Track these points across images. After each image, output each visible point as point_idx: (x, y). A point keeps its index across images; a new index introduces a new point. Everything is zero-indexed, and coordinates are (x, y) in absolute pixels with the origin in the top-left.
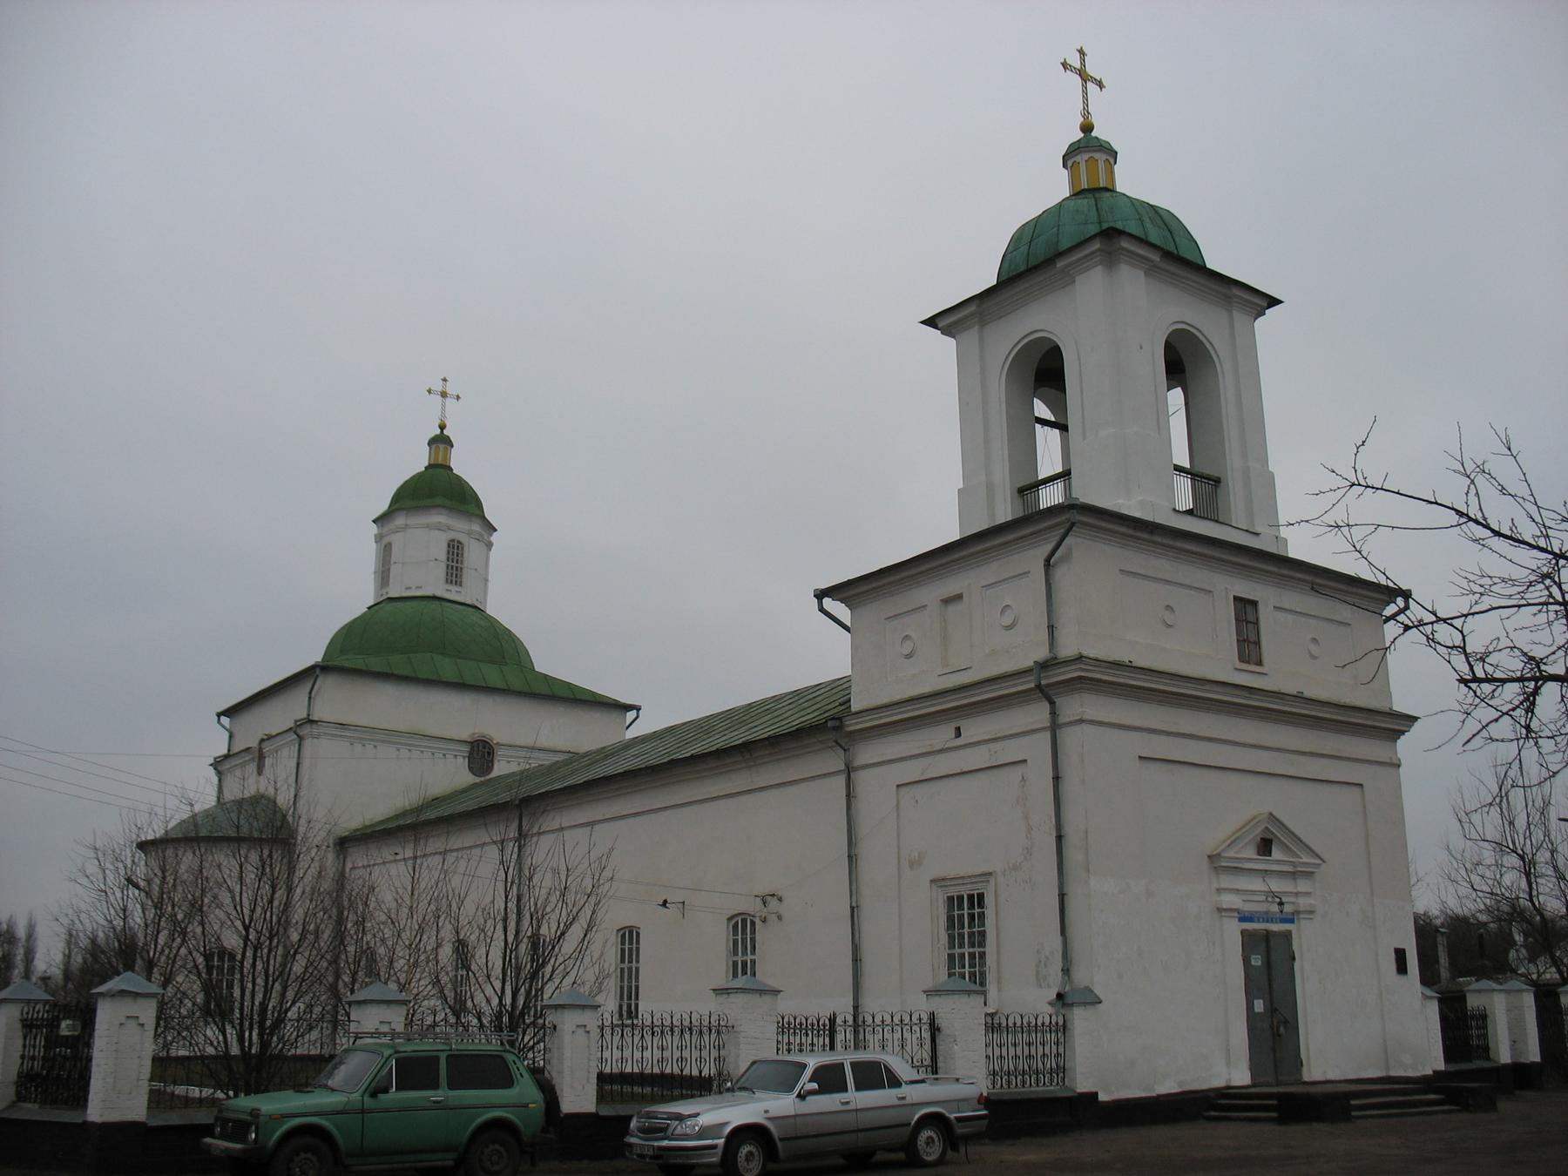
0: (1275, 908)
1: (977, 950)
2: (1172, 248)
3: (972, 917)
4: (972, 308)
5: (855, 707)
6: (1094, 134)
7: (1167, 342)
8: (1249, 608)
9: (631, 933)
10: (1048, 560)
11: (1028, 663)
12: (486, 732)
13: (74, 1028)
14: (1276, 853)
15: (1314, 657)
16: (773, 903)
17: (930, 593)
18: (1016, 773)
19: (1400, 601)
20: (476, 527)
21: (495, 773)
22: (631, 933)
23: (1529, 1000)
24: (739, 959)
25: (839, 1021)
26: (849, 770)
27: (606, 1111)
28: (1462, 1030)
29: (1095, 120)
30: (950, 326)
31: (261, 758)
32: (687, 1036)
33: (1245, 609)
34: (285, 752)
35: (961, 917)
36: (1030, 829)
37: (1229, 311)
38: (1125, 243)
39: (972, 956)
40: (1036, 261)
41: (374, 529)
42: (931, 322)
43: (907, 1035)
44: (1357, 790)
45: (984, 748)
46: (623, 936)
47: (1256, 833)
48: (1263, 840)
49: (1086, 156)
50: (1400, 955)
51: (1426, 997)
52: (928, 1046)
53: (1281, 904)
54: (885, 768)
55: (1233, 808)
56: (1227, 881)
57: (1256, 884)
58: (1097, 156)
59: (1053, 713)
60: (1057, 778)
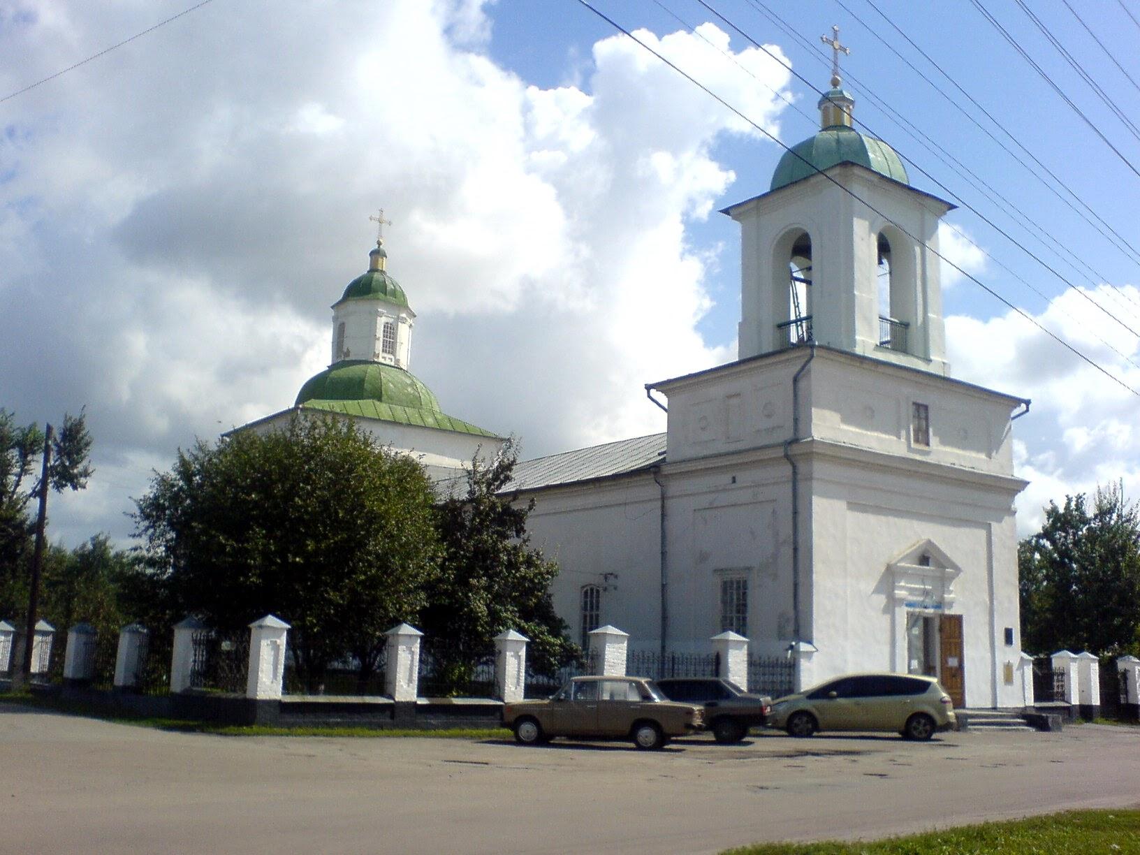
4: (752, 205)
10: (795, 380)
11: (781, 440)
19: (1023, 406)
23: (1095, 667)
28: (1046, 683)
30: (740, 214)
42: (726, 211)
50: (1008, 635)
59: (795, 473)
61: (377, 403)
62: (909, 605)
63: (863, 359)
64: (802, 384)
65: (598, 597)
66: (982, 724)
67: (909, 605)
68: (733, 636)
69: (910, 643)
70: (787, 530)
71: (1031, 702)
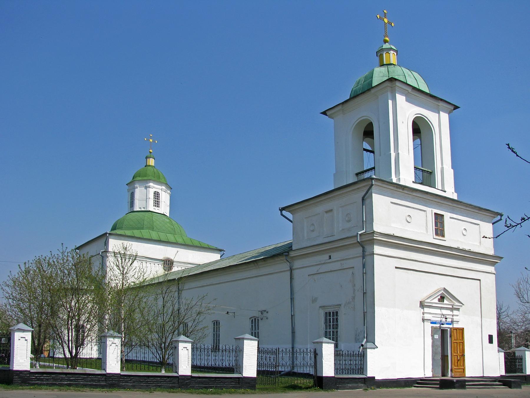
0: (444, 320)
1: (335, 330)
2: (416, 86)
3: (333, 319)
5: (294, 248)
7: (413, 122)
9: (217, 322)
10: (363, 199)
13: (5, 340)
14: (446, 301)
15: (465, 235)
16: (265, 313)
17: (320, 208)
18: (350, 271)
19: (499, 217)
21: (173, 270)
22: (217, 322)
25: (280, 350)
26: (291, 270)
32: (224, 353)
33: (439, 218)
35: (330, 319)
36: (354, 290)
38: (398, 84)
39: (333, 332)
42: (324, 113)
46: (214, 323)
51: (499, 351)
53: (446, 318)
55: (432, 285)
56: (426, 310)
57: (438, 311)
61: (151, 231)
63: (404, 187)
64: (367, 202)
65: (258, 323)
68: (182, 338)
69: (433, 343)
71: (503, 373)
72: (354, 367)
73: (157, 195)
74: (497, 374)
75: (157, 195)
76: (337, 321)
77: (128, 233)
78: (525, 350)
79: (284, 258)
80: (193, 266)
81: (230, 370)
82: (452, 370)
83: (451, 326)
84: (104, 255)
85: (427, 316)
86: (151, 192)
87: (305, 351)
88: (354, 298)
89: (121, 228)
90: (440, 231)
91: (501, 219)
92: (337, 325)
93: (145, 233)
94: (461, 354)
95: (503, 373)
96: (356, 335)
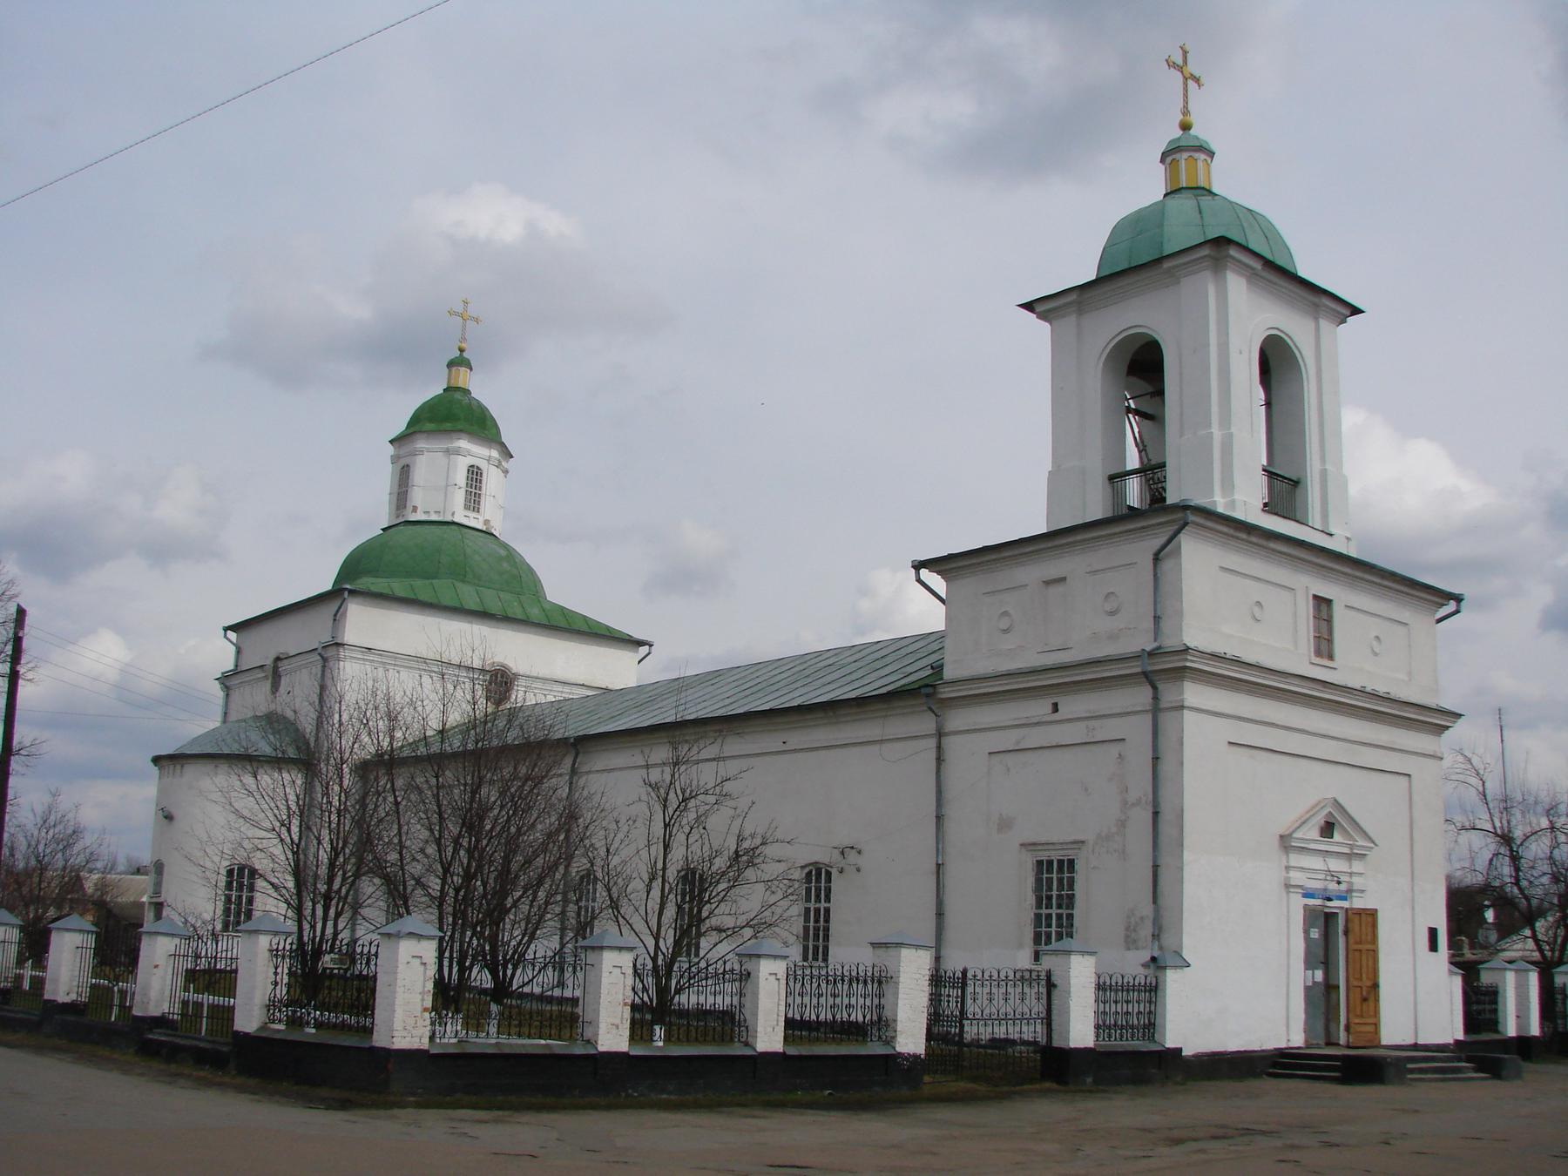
1: (1064, 912)
3: (1060, 881)
4: (1073, 297)
5: (948, 674)
6: (1192, 132)
8: (1324, 607)
10: (1157, 558)
12: (499, 659)
14: (1337, 837)
17: (1031, 573)
18: (1114, 750)
19: (1452, 606)
20: (495, 454)
24: (812, 905)
25: (969, 975)
26: (940, 734)
27: (792, 1051)
29: (1193, 118)
31: (276, 677)
33: (1322, 603)
34: (305, 674)
35: (1050, 880)
36: (1124, 802)
37: (1316, 319)
38: (1233, 252)
39: (1059, 917)
40: (1137, 262)
41: (391, 449)
42: (1028, 306)
43: (1027, 990)
44: (1404, 780)
45: (1082, 725)
47: (1320, 819)
48: (1327, 823)
49: (1185, 155)
50: (1433, 933)
52: (1044, 1001)
54: (976, 736)
55: (1311, 789)
56: (1296, 859)
57: (1315, 863)
58: (1196, 155)
59: (1156, 698)
60: (1156, 759)
61: (458, 584)
62: (1308, 895)
64: (1167, 565)
65: (829, 880)
66: (1421, 1071)
67: (1308, 895)
70: (1140, 785)
71: (1460, 1036)
72: (823, 986)
73: (475, 475)
74: (1448, 1039)
75: (475, 475)
76: (1071, 887)
77: (398, 587)
78: (1528, 970)
79: (924, 700)
80: (590, 693)
81: (855, 1031)
82: (1347, 1028)
83: (1346, 904)
84: (330, 653)
85: (1297, 877)
86: (462, 464)
87: (995, 976)
88: (1122, 824)
89: (374, 572)
90: (1324, 646)
91: (1457, 612)
92: (1071, 898)
93: (444, 590)
94: (1369, 983)
95: (1460, 1036)
96: (1127, 929)
